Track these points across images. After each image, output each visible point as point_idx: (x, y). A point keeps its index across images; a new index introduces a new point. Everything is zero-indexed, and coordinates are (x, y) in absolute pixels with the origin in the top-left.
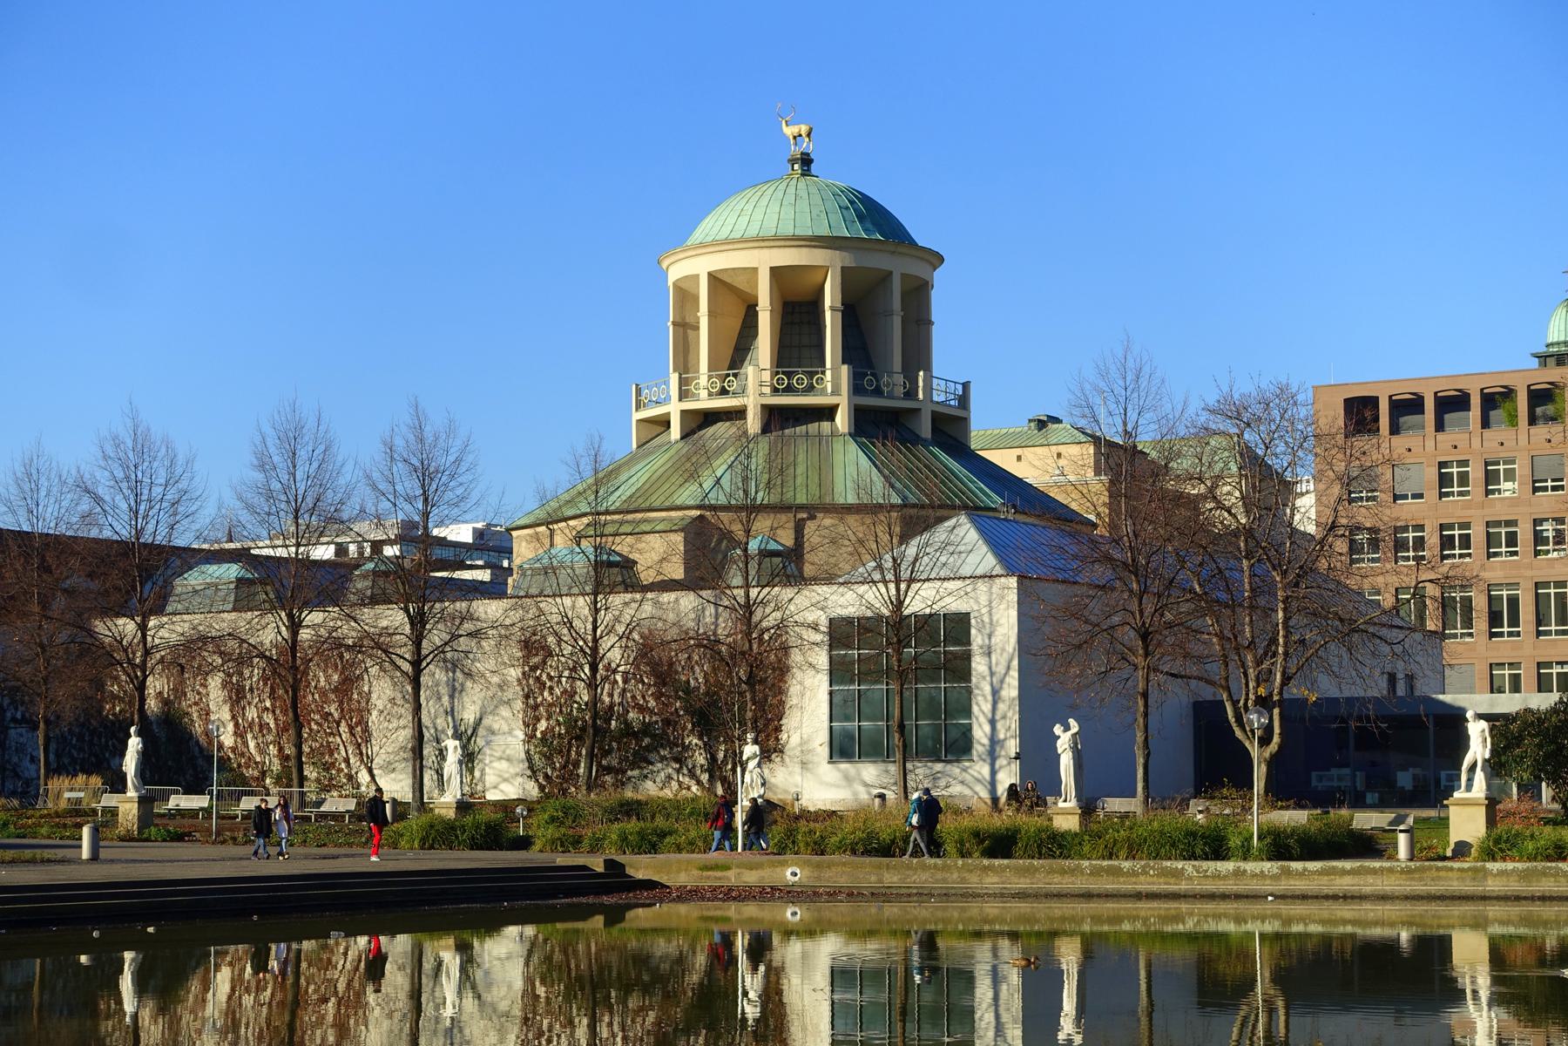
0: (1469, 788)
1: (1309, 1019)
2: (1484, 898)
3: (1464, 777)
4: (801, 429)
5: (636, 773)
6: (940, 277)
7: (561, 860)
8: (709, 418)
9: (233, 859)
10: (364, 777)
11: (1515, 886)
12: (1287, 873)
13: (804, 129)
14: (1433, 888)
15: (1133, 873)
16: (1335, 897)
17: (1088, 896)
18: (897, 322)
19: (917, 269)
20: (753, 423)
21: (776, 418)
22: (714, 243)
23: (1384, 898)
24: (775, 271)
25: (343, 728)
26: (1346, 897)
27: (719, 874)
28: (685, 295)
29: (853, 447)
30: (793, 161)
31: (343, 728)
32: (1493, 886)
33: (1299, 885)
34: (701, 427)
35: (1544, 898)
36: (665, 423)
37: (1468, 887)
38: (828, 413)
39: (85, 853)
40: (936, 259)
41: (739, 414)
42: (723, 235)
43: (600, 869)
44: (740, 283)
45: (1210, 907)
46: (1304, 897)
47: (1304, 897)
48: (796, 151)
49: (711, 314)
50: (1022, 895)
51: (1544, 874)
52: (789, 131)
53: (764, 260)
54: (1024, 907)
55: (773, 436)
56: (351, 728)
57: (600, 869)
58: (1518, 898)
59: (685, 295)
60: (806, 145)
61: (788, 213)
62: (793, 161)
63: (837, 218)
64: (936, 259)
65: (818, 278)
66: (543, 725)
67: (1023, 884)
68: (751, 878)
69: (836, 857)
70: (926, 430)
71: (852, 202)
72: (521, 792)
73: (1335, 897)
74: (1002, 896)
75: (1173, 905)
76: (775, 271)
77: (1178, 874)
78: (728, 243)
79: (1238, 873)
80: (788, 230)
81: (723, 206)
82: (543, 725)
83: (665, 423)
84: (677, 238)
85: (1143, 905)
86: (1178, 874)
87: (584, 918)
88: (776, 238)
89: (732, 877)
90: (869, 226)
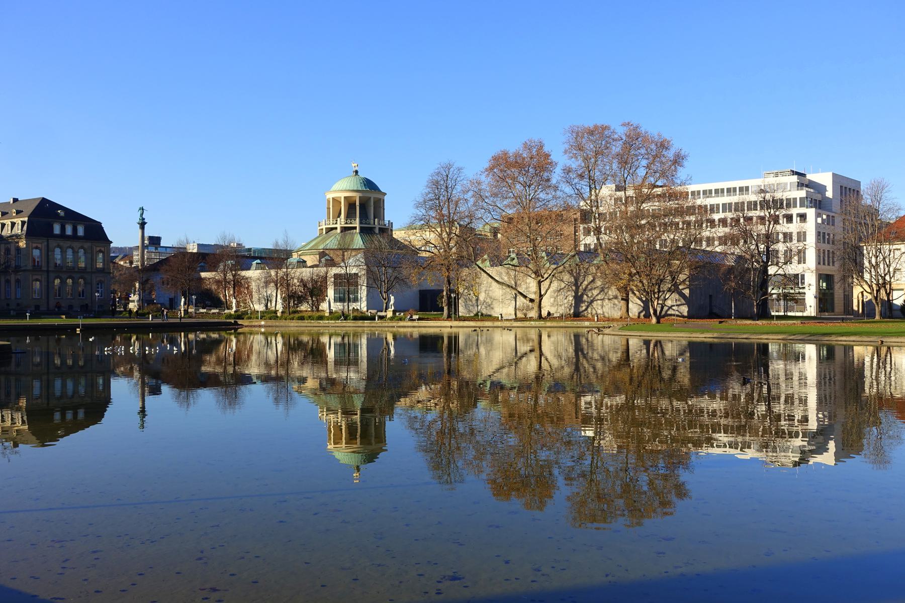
0: (391, 308)
1: (815, 385)
2: (364, 327)
3: (390, 307)
4: (349, 232)
5: (300, 305)
6: (386, 198)
7: (228, 321)
8: (332, 229)
9: (612, 335)
10: (252, 306)
11: (368, 325)
12: (336, 323)
14: (357, 325)
15: (313, 323)
16: (342, 327)
17: (306, 326)
18: (372, 208)
19: (379, 196)
20: (339, 230)
21: (344, 229)
22: (335, 191)
23: (350, 327)
25: (248, 296)
26: (344, 327)
27: (827, 338)
28: (329, 202)
30: (354, 172)
31: (248, 296)
32: (365, 325)
33: (337, 325)
34: (330, 231)
35: (373, 327)
36: (322, 229)
37: (362, 325)
38: (355, 228)
39: (150, 319)
41: (336, 228)
42: (341, 189)
43: (233, 322)
44: (339, 199)
45: (325, 328)
46: (338, 327)
47: (338, 327)
48: (354, 169)
49: (333, 206)
50: (297, 326)
51: (373, 323)
52: (353, 165)
53: (342, 195)
54: (297, 328)
55: (343, 233)
56: (249, 295)
57: (233, 322)
58: (369, 327)
61: (349, 184)
62: (354, 172)
63: (359, 185)
65: (355, 199)
66: (284, 295)
67: (297, 325)
68: (256, 324)
69: (254, 320)
70: (377, 231)
71: (363, 182)
73: (342, 327)
74: (294, 326)
75: (319, 328)
77: (320, 323)
78: (335, 191)
79: (329, 323)
80: (348, 188)
81: (337, 183)
82: (284, 295)
83: (322, 229)
84: (328, 190)
85: (315, 328)
86: (320, 323)
87: (231, 330)
88: (349, 190)
89: (254, 324)
90: (366, 187)
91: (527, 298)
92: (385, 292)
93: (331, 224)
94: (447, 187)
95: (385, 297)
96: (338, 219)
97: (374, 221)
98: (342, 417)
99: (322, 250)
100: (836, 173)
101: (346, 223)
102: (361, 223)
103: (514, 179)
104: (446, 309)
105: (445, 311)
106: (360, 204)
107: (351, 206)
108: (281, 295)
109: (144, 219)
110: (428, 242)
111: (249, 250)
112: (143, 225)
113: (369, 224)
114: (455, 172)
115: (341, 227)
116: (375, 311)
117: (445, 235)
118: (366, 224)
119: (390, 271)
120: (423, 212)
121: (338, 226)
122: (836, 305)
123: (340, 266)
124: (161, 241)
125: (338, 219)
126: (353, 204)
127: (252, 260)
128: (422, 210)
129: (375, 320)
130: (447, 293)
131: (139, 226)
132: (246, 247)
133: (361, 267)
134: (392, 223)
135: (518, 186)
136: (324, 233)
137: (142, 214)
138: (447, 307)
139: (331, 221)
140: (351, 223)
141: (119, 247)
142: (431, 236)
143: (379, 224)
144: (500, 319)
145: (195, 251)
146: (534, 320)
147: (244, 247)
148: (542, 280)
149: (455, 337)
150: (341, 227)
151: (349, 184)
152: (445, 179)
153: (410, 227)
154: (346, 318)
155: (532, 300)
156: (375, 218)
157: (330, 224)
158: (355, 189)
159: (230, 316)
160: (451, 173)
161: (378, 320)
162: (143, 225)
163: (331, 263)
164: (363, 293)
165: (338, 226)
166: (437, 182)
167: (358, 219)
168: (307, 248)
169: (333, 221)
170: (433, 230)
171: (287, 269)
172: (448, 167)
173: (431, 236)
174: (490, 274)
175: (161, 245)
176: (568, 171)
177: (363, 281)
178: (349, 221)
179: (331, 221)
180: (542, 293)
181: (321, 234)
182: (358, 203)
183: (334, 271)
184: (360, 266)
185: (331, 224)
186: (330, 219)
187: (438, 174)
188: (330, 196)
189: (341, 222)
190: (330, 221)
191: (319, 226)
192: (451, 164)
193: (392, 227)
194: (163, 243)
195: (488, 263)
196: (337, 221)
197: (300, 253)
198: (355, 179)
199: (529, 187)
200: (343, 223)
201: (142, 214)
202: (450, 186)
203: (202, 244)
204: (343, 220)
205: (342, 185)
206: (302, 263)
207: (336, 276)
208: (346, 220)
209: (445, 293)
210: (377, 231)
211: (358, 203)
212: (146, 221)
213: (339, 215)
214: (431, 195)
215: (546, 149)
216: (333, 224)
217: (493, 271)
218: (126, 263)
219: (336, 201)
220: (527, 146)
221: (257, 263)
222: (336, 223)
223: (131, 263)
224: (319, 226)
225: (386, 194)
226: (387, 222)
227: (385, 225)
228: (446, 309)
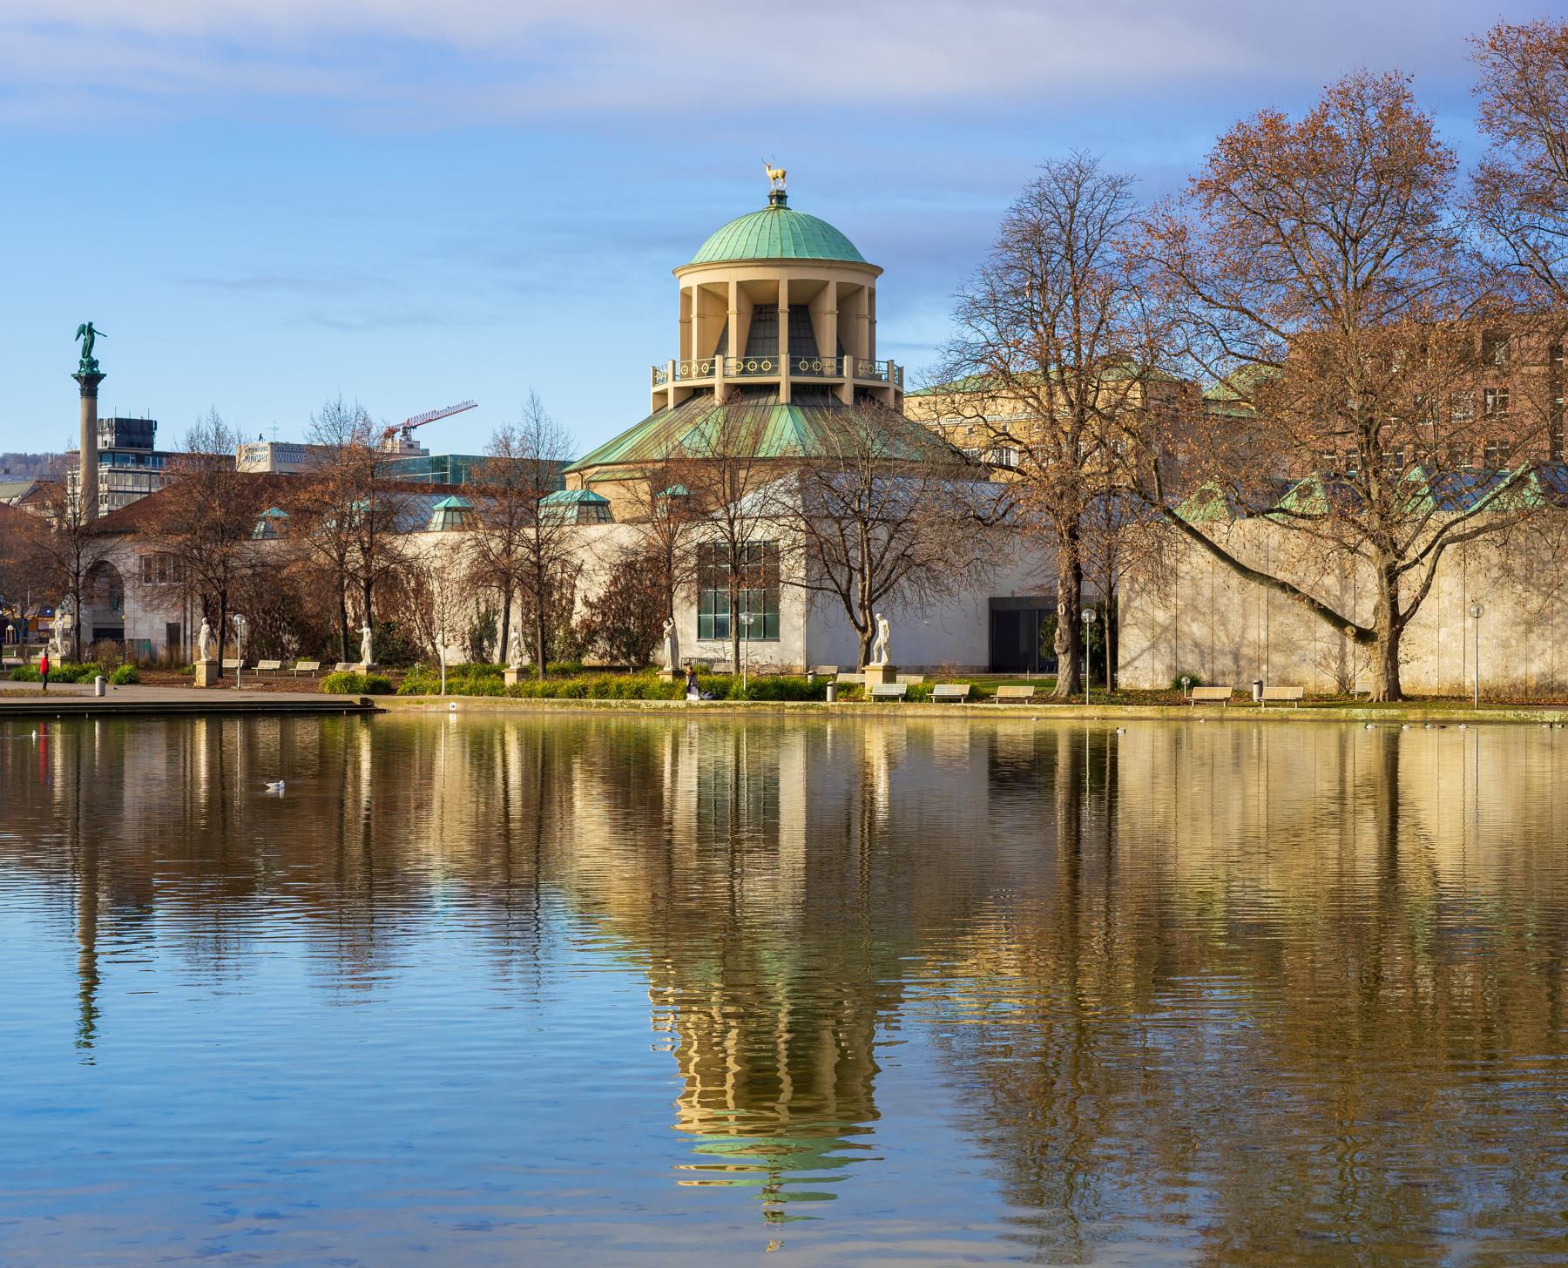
0: (879, 661)
3: (875, 654)
6: (880, 284)
8: (697, 392)
13: (780, 172)
20: (718, 392)
21: (739, 392)
24: (740, 285)
25: (418, 616)
28: (686, 296)
29: (786, 413)
30: (771, 197)
36: (664, 394)
38: (773, 388)
40: (876, 271)
42: (726, 257)
43: (358, 703)
44: (719, 291)
48: (773, 188)
53: (733, 277)
57: (358, 703)
59: (686, 296)
60: (781, 185)
61: (753, 240)
62: (771, 197)
63: (789, 243)
64: (876, 271)
70: (847, 396)
72: (1500, 671)
76: (740, 285)
80: (750, 255)
83: (664, 394)
91: (1348, 630)
92: (862, 606)
93: (694, 374)
94: (1069, 247)
95: (862, 624)
96: (718, 359)
97: (840, 362)
98: (725, 1016)
99: (659, 466)
100: (282, 440)
101: (744, 372)
102: (794, 371)
103: (1303, 216)
104: (1064, 661)
105: (1060, 672)
106: (790, 306)
107: (760, 311)
108: (525, 615)
109: (94, 364)
110: (1002, 439)
111: (439, 463)
112: (90, 381)
113: (821, 374)
114: (1099, 195)
115: (727, 385)
116: (832, 670)
117: (1064, 413)
118: (810, 372)
119: (881, 533)
120: (988, 333)
121: (716, 381)
122: (784, 837)
123: (712, 519)
124: (157, 433)
125: (718, 359)
126: (767, 306)
127: (435, 498)
128: (983, 326)
129: (824, 699)
130: (1068, 610)
131: (78, 385)
132: (433, 454)
133: (783, 521)
134: (901, 370)
135: (1320, 241)
136: (671, 405)
137: (88, 349)
138: (1068, 656)
139: (694, 366)
140: (760, 372)
141: (29, 454)
142: (1007, 411)
143: (855, 375)
144: (1255, 697)
145: (263, 467)
146: (1372, 704)
147: (426, 452)
148: (1401, 563)
149: (1098, 753)
150: (727, 385)
151: (754, 238)
152: (1065, 218)
153: (943, 389)
154: (719, 692)
155: (1364, 636)
156: (841, 352)
157: (689, 375)
158: (776, 254)
159: (350, 684)
160: (1085, 198)
161: (834, 699)
162: (90, 381)
163: (692, 509)
164: (792, 606)
165: (716, 381)
166: (1038, 230)
167: (784, 359)
168: (612, 458)
169: (700, 364)
170: (1022, 392)
171: (537, 526)
172: (1076, 176)
173: (1007, 411)
174: (1221, 546)
175: (157, 448)
176: (1492, 182)
177: (793, 567)
178: (753, 365)
179: (694, 366)
180: (1403, 608)
181: (659, 410)
182: (783, 304)
183: (700, 534)
184: (777, 517)
185: (694, 374)
186: (689, 357)
187: (1043, 199)
188: (692, 281)
189: (728, 369)
190: (689, 365)
191: (655, 383)
192: (1085, 164)
193: (901, 384)
194: (161, 443)
195: (1218, 506)
196: (713, 364)
197: (589, 473)
198: (776, 221)
199: (1355, 241)
200: (733, 372)
201: (88, 349)
202: (1081, 244)
203: (287, 445)
204: (732, 363)
205: (733, 243)
206: (596, 510)
207: (704, 552)
208: (745, 362)
209: (1061, 609)
210: (847, 396)
211: (783, 304)
212: (101, 369)
213: (721, 348)
214: (1014, 276)
215: (1418, 108)
216: (700, 374)
217: (1241, 535)
218: (44, 507)
219: (712, 296)
220: (1348, 99)
221: (447, 509)
222: (711, 373)
223: (60, 508)
224: (655, 383)
225: (881, 271)
226: (884, 367)
227: (879, 378)
228: (1064, 661)
